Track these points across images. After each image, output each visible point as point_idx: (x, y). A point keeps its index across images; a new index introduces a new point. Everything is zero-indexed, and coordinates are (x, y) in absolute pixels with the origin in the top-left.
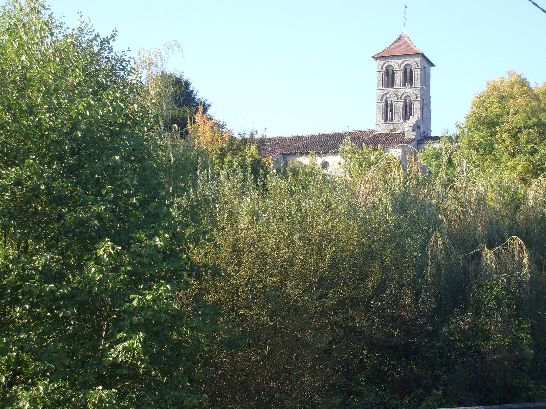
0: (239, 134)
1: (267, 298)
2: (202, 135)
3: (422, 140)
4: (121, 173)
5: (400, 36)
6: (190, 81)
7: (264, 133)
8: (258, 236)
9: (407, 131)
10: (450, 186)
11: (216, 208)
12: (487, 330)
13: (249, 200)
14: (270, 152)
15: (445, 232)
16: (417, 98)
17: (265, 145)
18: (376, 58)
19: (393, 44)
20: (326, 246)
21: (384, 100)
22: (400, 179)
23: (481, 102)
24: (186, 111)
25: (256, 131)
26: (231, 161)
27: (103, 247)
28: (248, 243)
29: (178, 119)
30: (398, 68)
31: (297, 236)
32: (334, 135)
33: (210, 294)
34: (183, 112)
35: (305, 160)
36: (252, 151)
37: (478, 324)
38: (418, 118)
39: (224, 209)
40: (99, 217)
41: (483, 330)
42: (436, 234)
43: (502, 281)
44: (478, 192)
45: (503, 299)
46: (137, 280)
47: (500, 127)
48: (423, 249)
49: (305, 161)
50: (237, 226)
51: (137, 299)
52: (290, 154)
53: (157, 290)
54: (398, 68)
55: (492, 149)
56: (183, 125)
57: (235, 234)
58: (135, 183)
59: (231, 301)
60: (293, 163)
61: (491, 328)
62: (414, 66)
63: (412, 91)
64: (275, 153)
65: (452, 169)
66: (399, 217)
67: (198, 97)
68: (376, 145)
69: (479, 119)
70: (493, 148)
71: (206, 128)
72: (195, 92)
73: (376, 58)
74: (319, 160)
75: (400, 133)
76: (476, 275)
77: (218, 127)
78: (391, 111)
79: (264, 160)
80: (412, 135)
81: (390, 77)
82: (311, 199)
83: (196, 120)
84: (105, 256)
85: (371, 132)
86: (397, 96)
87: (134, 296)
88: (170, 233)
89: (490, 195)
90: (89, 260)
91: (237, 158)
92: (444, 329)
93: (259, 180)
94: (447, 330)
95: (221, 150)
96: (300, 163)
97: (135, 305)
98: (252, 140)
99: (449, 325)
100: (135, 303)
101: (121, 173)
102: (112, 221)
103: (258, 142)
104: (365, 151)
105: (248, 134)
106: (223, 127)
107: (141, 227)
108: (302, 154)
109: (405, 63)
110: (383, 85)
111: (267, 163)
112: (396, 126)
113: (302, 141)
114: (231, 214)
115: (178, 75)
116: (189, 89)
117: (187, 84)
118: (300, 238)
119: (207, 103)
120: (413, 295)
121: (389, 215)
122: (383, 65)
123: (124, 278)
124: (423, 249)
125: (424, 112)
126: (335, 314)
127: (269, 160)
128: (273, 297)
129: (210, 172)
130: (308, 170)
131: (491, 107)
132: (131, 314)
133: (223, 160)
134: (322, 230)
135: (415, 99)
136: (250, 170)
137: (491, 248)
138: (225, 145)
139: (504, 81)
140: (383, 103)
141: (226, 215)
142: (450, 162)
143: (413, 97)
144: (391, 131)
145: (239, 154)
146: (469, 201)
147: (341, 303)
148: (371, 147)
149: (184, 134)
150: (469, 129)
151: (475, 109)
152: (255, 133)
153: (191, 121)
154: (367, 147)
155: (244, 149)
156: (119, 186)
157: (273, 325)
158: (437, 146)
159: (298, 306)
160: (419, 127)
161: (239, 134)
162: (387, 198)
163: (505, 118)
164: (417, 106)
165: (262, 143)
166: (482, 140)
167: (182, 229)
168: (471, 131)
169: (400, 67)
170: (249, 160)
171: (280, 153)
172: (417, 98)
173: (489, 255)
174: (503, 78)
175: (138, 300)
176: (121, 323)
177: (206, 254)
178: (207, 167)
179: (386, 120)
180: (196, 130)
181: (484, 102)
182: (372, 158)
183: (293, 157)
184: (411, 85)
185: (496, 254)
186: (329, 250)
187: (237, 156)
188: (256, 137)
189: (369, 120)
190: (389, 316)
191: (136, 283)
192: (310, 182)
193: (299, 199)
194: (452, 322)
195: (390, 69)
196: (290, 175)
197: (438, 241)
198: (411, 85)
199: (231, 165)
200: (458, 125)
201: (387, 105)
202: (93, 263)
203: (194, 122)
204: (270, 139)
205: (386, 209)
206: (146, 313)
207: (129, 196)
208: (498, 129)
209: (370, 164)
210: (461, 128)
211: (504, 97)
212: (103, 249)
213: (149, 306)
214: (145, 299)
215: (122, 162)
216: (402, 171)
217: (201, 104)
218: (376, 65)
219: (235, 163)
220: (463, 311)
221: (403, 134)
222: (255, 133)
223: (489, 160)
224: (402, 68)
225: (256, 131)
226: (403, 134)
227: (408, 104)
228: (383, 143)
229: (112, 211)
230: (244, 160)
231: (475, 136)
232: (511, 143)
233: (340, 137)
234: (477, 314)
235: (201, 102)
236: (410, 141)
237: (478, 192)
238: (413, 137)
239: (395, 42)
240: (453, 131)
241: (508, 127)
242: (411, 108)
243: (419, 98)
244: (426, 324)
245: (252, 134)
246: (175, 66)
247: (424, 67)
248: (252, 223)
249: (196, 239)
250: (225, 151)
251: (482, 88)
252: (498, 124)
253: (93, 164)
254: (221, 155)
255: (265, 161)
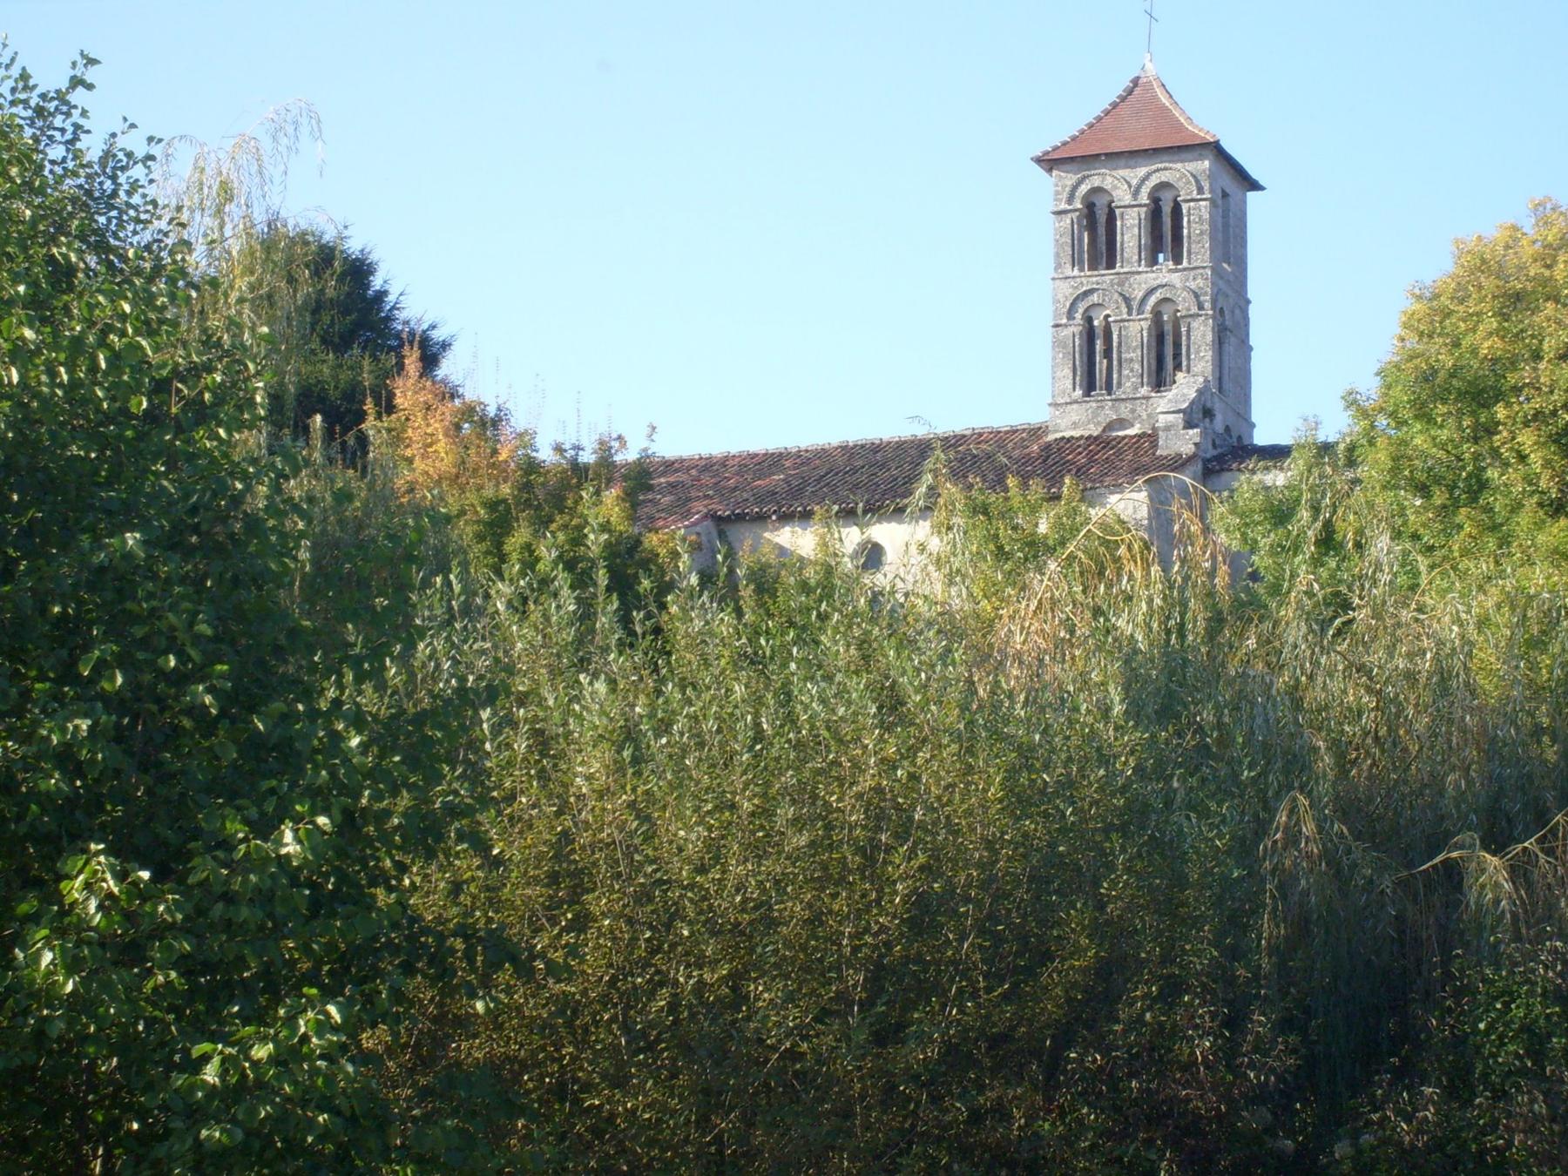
0: (559, 449)
1: (686, 1049)
2: (417, 453)
3: (1219, 458)
4: (150, 596)
5: (1136, 82)
6: (373, 257)
7: (645, 444)
8: (645, 818)
9: (1167, 428)
10: (1338, 622)
11: (482, 722)
12: (1495, 1148)
13: (601, 687)
14: (670, 510)
15: (1324, 788)
16: (1201, 307)
17: (650, 488)
18: (1049, 162)
19: (1107, 113)
20: (889, 849)
21: (1078, 316)
22: (1150, 601)
23: (1435, 316)
24: (361, 368)
25: (620, 438)
26: (528, 548)
27: (80, 872)
28: (608, 845)
29: (333, 394)
30: (1127, 199)
31: (786, 812)
32: (901, 447)
33: (475, 1036)
34: (351, 368)
35: (800, 540)
36: (606, 509)
37: (1461, 1129)
38: (1206, 381)
39: (514, 724)
40: (66, 759)
41: (1482, 1153)
42: (1295, 799)
43: (1546, 967)
44: (1440, 643)
45: (1550, 1036)
46: (224, 988)
47: (1508, 405)
48: (1244, 849)
49: (800, 541)
50: (566, 786)
51: (216, 1060)
52: (740, 518)
53: (291, 1021)
54: (1127, 199)
55: (1478, 486)
56: (345, 417)
57: (559, 813)
58: (204, 629)
59: (554, 1060)
60: (754, 549)
61: (1509, 1144)
62: (1186, 191)
63: (1181, 283)
64: (687, 515)
65: (1333, 565)
66: (1153, 736)
67: (402, 315)
68: (1055, 480)
69: (1428, 377)
70: (1483, 485)
71: (436, 426)
72: (391, 298)
73: (1049, 162)
74: (851, 537)
75: (1140, 436)
76: (1446, 948)
77: (488, 424)
78: (1108, 353)
79: (652, 540)
80: (1185, 442)
81: (1102, 230)
82: (829, 678)
83: (399, 400)
84: (93, 905)
85: (1036, 432)
86: (1127, 300)
87: (205, 1047)
88: (336, 811)
89: (1488, 654)
90: (35, 919)
91: (553, 533)
92: (1341, 1149)
93: (638, 616)
94: (1349, 1151)
95: (492, 505)
96: (782, 551)
97: (210, 1079)
98: (606, 470)
99: (1355, 1136)
100: (210, 1074)
101: (150, 596)
102: (117, 773)
103: (625, 478)
104: (1016, 502)
105: (589, 450)
106: (496, 422)
107: (231, 790)
108: (786, 518)
109: (1154, 180)
110: (1076, 261)
111: (663, 552)
112: (1124, 410)
113: (783, 470)
114: (542, 741)
115: (327, 238)
116: (368, 286)
117: (359, 270)
118: (797, 823)
119: (438, 335)
120: (1220, 1026)
121: (1116, 729)
122: (1075, 188)
123: (169, 983)
124: (1244, 849)
125: (1226, 358)
126: (935, 1099)
127: (672, 539)
128: (708, 1042)
129: (457, 588)
130: (811, 574)
131: (1474, 330)
132: (196, 1115)
133: (499, 545)
134: (878, 790)
135: (1194, 310)
136: (602, 578)
137: (1496, 842)
138: (506, 490)
139: (1516, 240)
140: (1076, 328)
141: (521, 746)
142: (1328, 541)
143: (1185, 304)
144: (1110, 426)
145: (559, 520)
146: (1411, 676)
147: (955, 1055)
148: (1037, 488)
149: (355, 453)
150: (1392, 415)
151: (1412, 342)
152: (616, 444)
153: (377, 404)
154: (1024, 485)
155: (576, 503)
156: (144, 643)
157: (709, 1144)
158: (1278, 478)
159: (796, 1074)
160: (1208, 413)
161: (559, 449)
162: (1106, 675)
163: (1525, 374)
164: (1201, 334)
165: (643, 481)
166: (1441, 454)
167: (377, 797)
168: (1401, 423)
169: (1136, 194)
170: (595, 541)
171: (705, 517)
172: (1201, 307)
173: (1491, 873)
174: (1515, 228)
175: (223, 1062)
176: (160, 1151)
177: (456, 888)
178: (445, 570)
179: (1089, 387)
180: (397, 438)
181: (1448, 314)
182: (1043, 528)
183: (756, 528)
184: (1177, 259)
185: (1520, 871)
186: (902, 866)
187: (553, 526)
188: (619, 458)
189: (1024, 389)
190: (1135, 1103)
191: (216, 997)
192: (824, 617)
193: (787, 683)
194: (1369, 1123)
195: (1100, 202)
196: (747, 592)
197: (1301, 822)
198: (1177, 259)
199: (530, 561)
200: (1351, 401)
201: (1090, 334)
202: (45, 932)
203: (390, 408)
204: (669, 466)
205: (1106, 711)
206: (253, 1112)
207: (181, 679)
208: (1501, 412)
209: (1036, 550)
210: (1364, 414)
211: (1518, 297)
212: (81, 877)
213: (260, 1084)
214: (248, 1058)
215: (149, 557)
216: (1155, 570)
217: (411, 343)
218: (1047, 189)
219: (547, 554)
220: (1408, 1075)
221: (1151, 438)
222: (616, 444)
223: (1467, 529)
224: (1144, 198)
225: (620, 438)
226: (1151, 438)
227: (1168, 328)
228: (1080, 473)
229: (120, 737)
230: (578, 540)
231: (1418, 441)
232: (1547, 464)
233: (913, 453)
234: (1458, 1089)
235: (412, 333)
236: (1178, 463)
237: (1440, 643)
238: (1187, 449)
239: (1115, 105)
240: (1336, 426)
241: (1537, 403)
242: (1177, 345)
243: (1207, 305)
244: (1270, 1131)
245: (605, 449)
246: (322, 198)
247: (1225, 195)
248: (620, 768)
249: (425, 836)
250: (508, 510)
251: (1436, 265)
252: (1499, 396)
253: (42, 561)
254: (490, 525)
255: (658, 541)
